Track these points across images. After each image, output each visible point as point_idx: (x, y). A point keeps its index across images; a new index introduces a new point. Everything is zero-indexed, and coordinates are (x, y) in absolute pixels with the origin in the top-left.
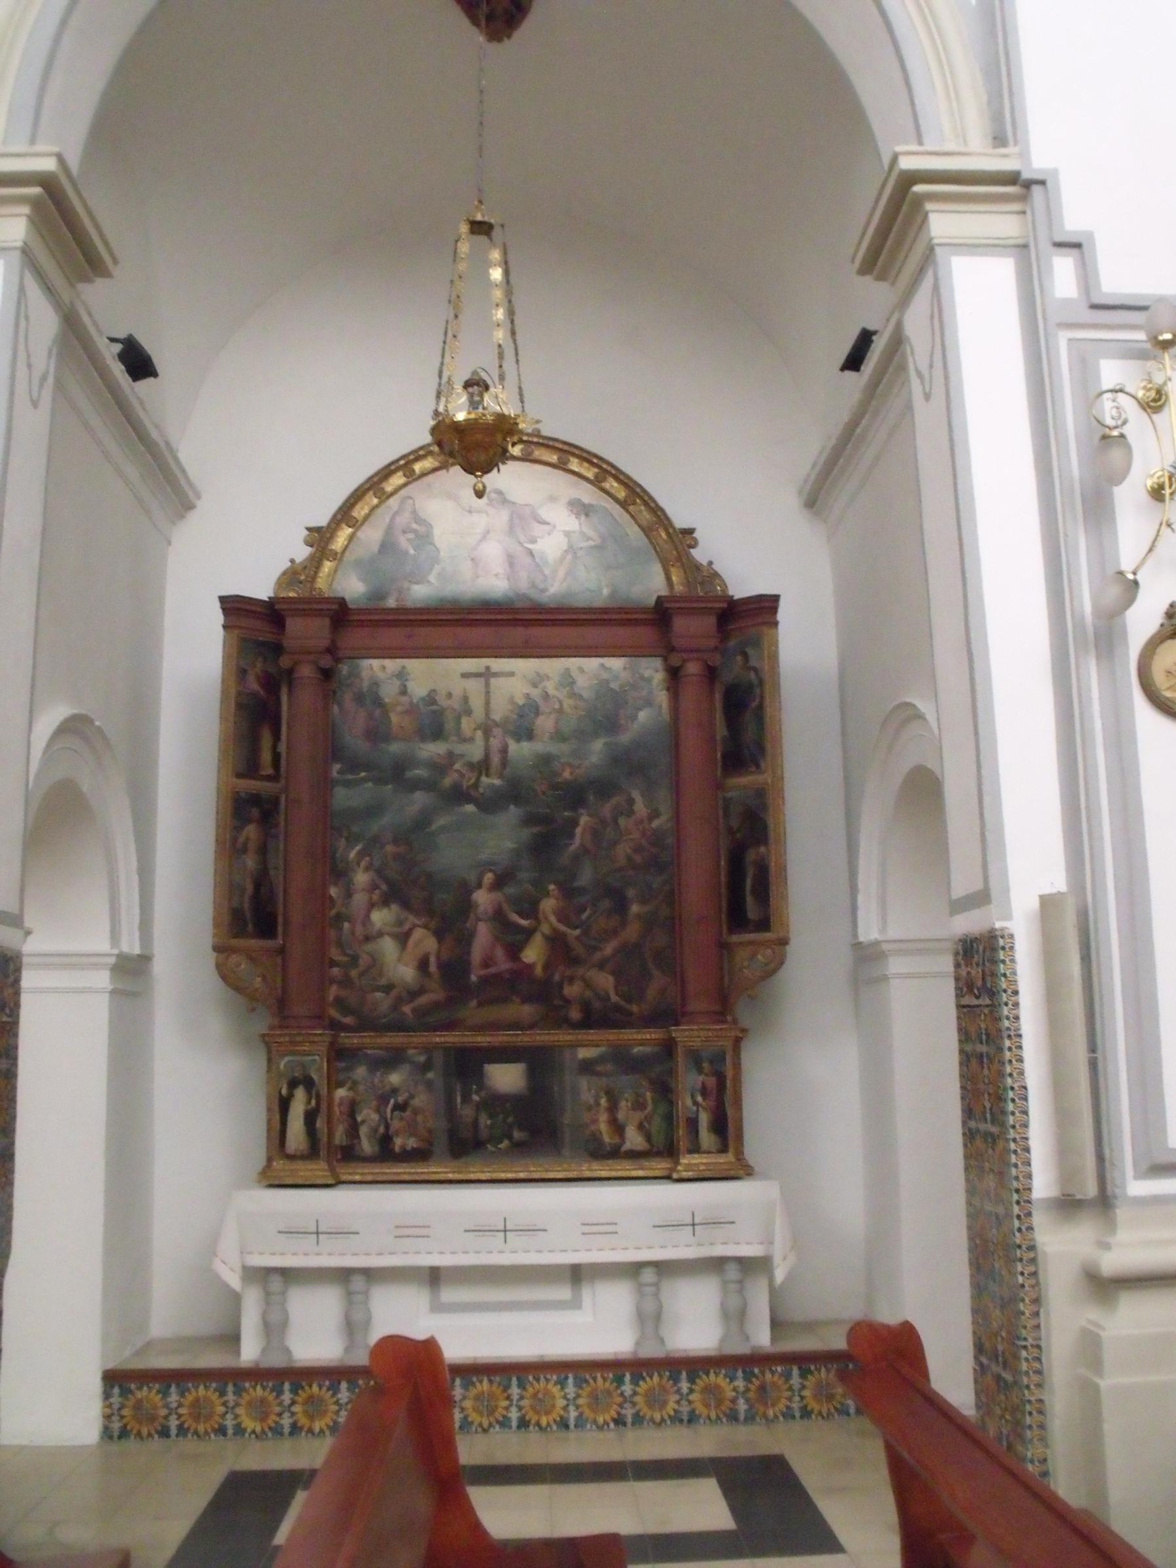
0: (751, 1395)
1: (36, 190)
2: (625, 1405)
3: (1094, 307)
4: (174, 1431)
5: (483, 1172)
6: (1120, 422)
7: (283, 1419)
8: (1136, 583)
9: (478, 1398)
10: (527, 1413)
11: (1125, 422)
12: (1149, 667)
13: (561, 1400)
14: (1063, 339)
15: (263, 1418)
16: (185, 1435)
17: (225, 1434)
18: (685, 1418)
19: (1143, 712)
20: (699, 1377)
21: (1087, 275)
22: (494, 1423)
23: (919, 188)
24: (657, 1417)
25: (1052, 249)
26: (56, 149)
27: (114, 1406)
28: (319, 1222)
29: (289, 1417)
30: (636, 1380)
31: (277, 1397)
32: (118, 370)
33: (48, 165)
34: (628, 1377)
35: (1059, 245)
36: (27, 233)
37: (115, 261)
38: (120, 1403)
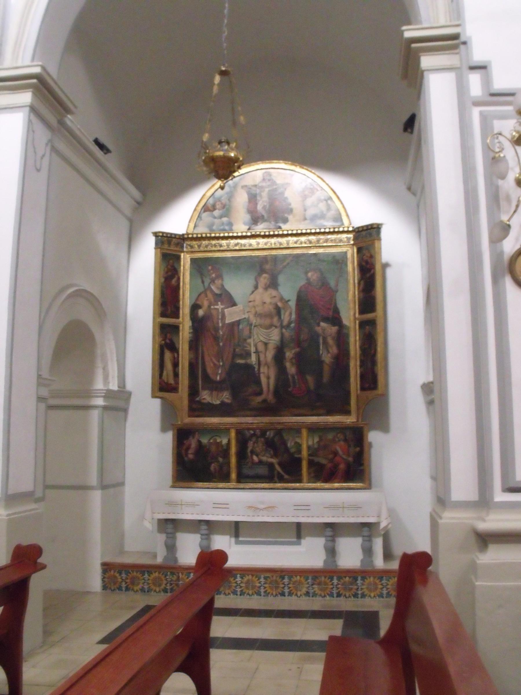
0: (128, 581)
1: (35, 81)
2: (237, 587)
3: (493, 95)
4: (287, 594)
5: (310, 485)
6: (501, 149)
7: (285, 589)
8: (509, 226)
9: (370, 584)
10: (173, 587)
11: (503, 149)
12: (515, 263)
13: (165, 581)
14: (476, 112)
15: (115, 583)
16: (244, 595)
17: (285, 596)
18: (146, 590)
19: (509, 284)
20: (367, 579)
21: (487, 81)
22: (326, 595)
23: (413, 45)
24: (158, 590)
25: (469, 71)
26: (40, 63)
27: (310, 583)
28: (214, 507)
29: (386, 590)
30: (363, 578)
31: (331, 581)
32: (95, 149)
33: (37, 70)
34: (359, 578)
35: (473, 68)
36: (32, 99)
37: (76, 107)
38: (337, 583)
